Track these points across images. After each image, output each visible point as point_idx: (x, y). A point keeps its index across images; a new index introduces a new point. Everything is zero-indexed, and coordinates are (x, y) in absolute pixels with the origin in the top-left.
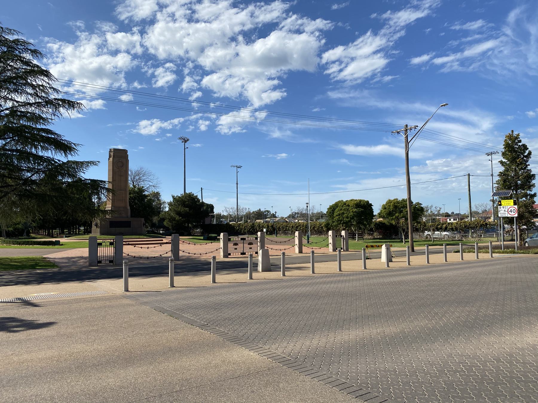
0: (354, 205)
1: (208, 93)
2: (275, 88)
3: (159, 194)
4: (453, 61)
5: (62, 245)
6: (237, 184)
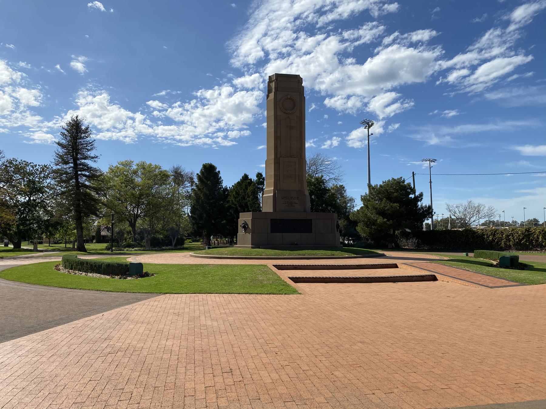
1: (332, 111)
3: (344, 187)
5: (147, 275)
6: (431, 182)
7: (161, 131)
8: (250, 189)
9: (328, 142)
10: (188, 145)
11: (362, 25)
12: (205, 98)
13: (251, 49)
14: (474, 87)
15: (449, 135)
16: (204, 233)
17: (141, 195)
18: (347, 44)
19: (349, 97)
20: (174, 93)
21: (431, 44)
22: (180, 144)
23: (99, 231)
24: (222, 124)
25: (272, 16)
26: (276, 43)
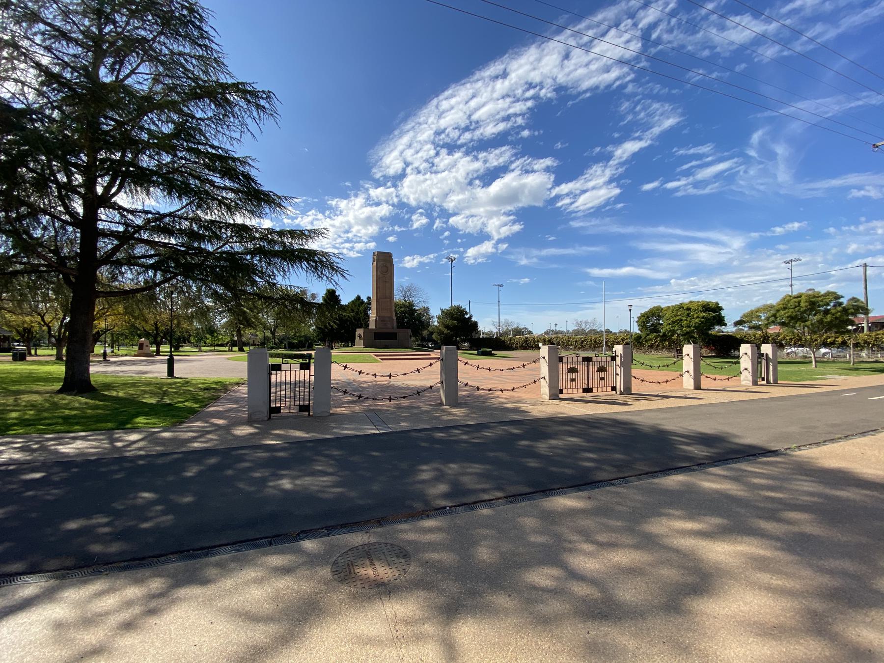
0: (700, 307)
1: (454, 230)
2: (514, 222)
4: (685, 185)
8: (361, 308)
15: (536, 257)
24: (350, 235)
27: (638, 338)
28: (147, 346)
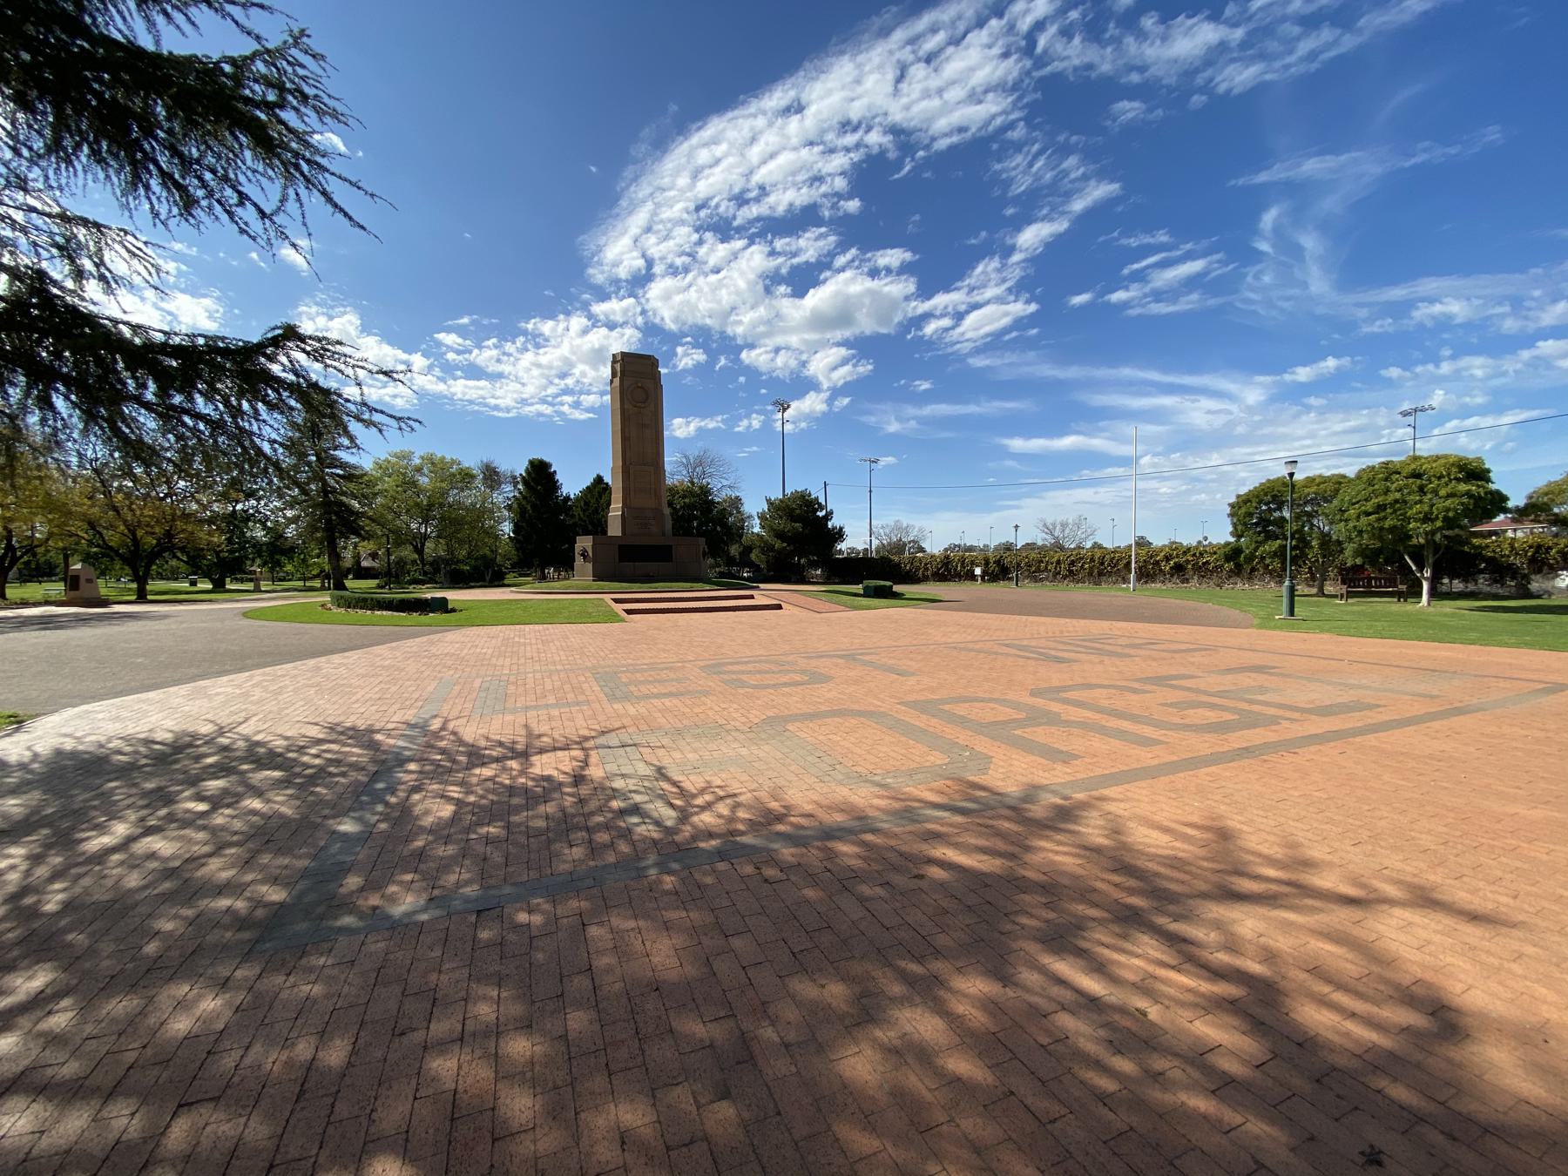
1: (752, 372)
5: (453, 610)
7: (461, 388)
9: (745, 423)
10: (511, 415)
11: (805, 231)
12: (541, 335)
13: (623, 253)
14: (958, 346)
16: (536, 563)
17: (430, 506)
18: (781, 260)
19: (777, 350)
20: (485, 322)
21: (905, 269)
22: (495, 413)
23: (357, 558)
24: (570, 381)
25: (659, 198)
26: (664, 247)
27: (1233, 553)
28: (89, 581)
